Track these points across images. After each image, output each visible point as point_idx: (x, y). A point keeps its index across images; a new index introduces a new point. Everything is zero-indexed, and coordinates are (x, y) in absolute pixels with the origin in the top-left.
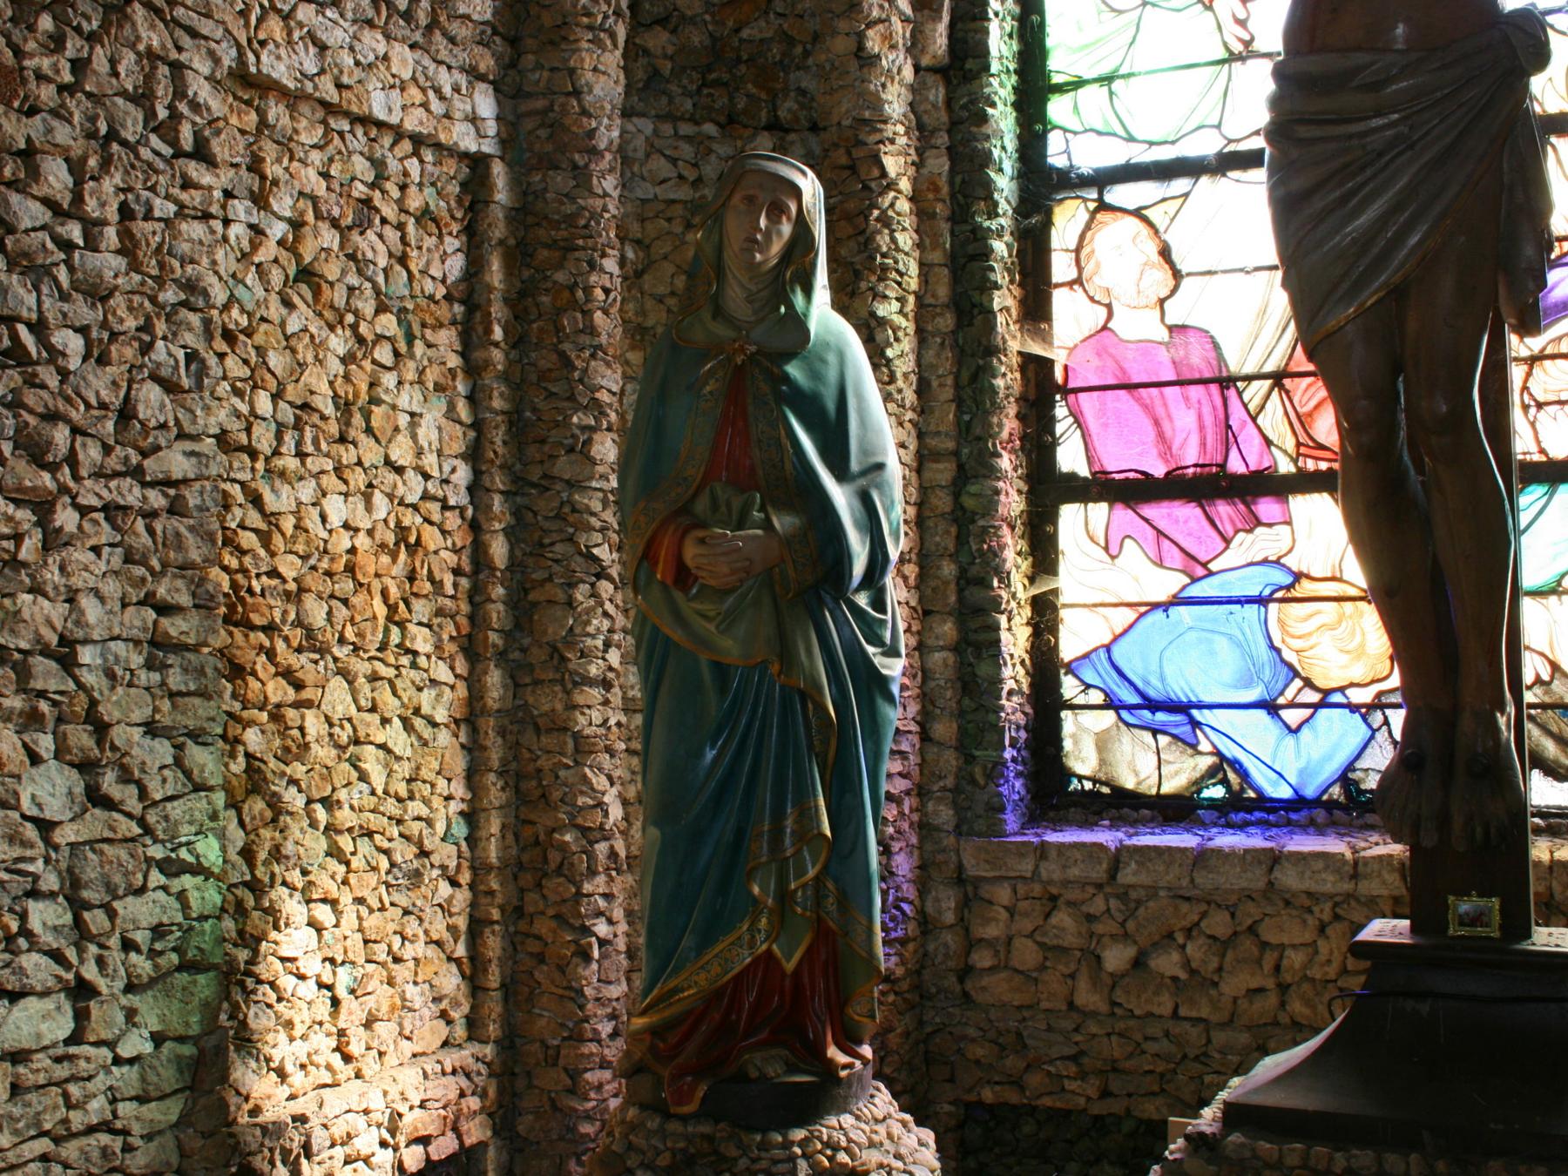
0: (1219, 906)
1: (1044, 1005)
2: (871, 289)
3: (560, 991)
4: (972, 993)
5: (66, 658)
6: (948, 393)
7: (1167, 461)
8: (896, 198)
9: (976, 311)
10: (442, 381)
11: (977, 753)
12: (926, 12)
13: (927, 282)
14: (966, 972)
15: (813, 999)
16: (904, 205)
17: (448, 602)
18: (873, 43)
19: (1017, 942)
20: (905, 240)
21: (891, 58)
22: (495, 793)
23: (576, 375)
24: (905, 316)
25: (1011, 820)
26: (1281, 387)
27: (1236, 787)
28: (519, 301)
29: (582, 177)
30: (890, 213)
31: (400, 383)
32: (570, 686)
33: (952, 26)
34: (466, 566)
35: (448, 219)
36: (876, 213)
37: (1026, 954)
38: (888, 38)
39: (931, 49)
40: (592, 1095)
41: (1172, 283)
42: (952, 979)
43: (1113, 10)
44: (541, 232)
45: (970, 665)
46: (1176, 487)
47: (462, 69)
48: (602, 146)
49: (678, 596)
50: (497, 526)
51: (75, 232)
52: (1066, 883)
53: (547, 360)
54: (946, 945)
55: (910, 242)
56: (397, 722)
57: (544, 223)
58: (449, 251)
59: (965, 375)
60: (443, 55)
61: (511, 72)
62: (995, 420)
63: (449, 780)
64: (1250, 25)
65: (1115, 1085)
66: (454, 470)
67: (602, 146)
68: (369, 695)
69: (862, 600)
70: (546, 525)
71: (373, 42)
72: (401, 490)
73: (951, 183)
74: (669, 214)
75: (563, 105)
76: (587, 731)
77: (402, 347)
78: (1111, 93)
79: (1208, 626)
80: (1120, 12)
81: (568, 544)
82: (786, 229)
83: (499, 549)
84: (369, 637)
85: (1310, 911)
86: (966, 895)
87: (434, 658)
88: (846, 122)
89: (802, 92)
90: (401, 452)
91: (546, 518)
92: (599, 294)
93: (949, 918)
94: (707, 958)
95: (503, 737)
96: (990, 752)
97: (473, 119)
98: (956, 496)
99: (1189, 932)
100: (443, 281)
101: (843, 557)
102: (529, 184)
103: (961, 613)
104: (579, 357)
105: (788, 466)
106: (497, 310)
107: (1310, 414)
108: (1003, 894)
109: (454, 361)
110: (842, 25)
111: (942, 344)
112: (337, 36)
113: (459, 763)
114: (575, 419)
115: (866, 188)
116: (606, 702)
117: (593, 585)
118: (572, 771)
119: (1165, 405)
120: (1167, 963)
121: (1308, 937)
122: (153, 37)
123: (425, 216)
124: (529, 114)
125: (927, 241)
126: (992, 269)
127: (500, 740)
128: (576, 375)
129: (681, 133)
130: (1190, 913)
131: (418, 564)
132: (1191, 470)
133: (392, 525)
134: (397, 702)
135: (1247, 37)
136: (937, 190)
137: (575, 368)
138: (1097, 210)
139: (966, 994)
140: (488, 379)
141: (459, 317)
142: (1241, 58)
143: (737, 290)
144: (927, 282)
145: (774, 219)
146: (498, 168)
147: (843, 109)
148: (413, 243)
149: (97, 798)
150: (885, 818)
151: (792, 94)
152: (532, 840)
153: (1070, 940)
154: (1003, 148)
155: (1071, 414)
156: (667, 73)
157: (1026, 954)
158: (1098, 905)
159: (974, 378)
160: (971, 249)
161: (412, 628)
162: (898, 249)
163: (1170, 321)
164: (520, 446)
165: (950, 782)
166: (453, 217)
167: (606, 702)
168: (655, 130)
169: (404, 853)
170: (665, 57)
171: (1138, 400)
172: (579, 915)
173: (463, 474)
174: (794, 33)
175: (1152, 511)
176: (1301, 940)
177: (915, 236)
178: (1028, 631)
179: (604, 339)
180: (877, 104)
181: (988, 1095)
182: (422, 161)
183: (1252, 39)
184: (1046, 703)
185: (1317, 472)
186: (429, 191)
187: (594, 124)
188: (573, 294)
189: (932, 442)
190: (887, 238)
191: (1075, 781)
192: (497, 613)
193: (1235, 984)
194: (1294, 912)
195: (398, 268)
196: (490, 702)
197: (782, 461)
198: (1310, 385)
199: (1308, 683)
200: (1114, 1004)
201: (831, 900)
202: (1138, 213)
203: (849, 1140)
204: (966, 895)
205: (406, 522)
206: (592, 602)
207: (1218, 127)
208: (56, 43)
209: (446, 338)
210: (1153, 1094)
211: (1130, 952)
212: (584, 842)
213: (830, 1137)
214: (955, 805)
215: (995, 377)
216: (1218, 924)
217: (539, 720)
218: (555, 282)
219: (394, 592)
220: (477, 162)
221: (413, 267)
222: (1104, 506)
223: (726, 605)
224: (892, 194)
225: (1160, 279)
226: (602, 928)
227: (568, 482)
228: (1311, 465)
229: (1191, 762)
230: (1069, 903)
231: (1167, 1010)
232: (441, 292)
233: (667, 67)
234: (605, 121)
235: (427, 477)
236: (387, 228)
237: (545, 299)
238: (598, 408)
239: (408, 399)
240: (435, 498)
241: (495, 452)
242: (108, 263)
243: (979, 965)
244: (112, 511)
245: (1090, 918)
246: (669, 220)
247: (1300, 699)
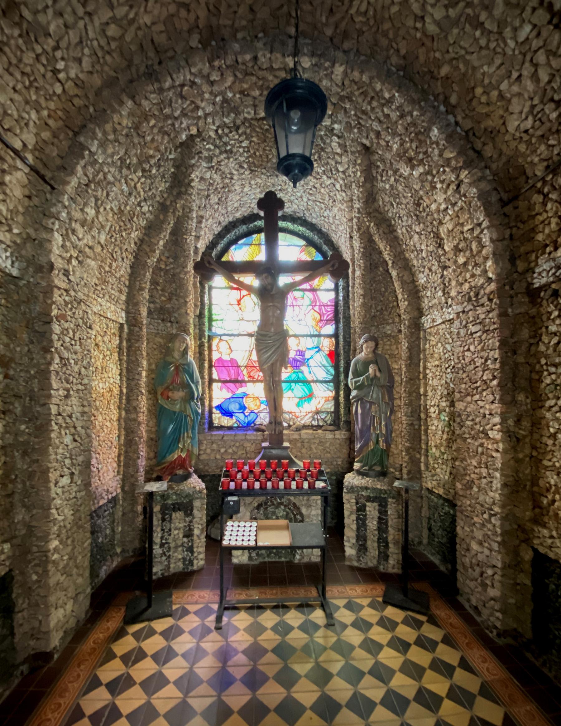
5: (70, 417)
22: (123, 432)
25: (206, 430)
28: (129, 348)
29: (141, 329)
37: (208, 451)
46: (230, 381)
51: (73, 342)
53: (134, 359)
71: (108, 304)
83: (125, 391)
90: (110, 375)
106: (125, 350)
112: (103, 304)
113: (117, 427)
120: (230, 451)
122: (84, 308)
123: (114, 334)
130: (233, 443)
146: (125, 327)
147: (183, 321)
149: (75, 440)
157: (208, 451)
164: (129, 373)
169: (109, 444)
184: (211, 413)
192: (124, 401)
193: (240, 453)
208: (71, 309)
209: (116, 354)
216: (237, 444)
220: (122, 325)
225: (229, 351)
239: (111, 366)
242: (78, 347)
244: (78, 390)
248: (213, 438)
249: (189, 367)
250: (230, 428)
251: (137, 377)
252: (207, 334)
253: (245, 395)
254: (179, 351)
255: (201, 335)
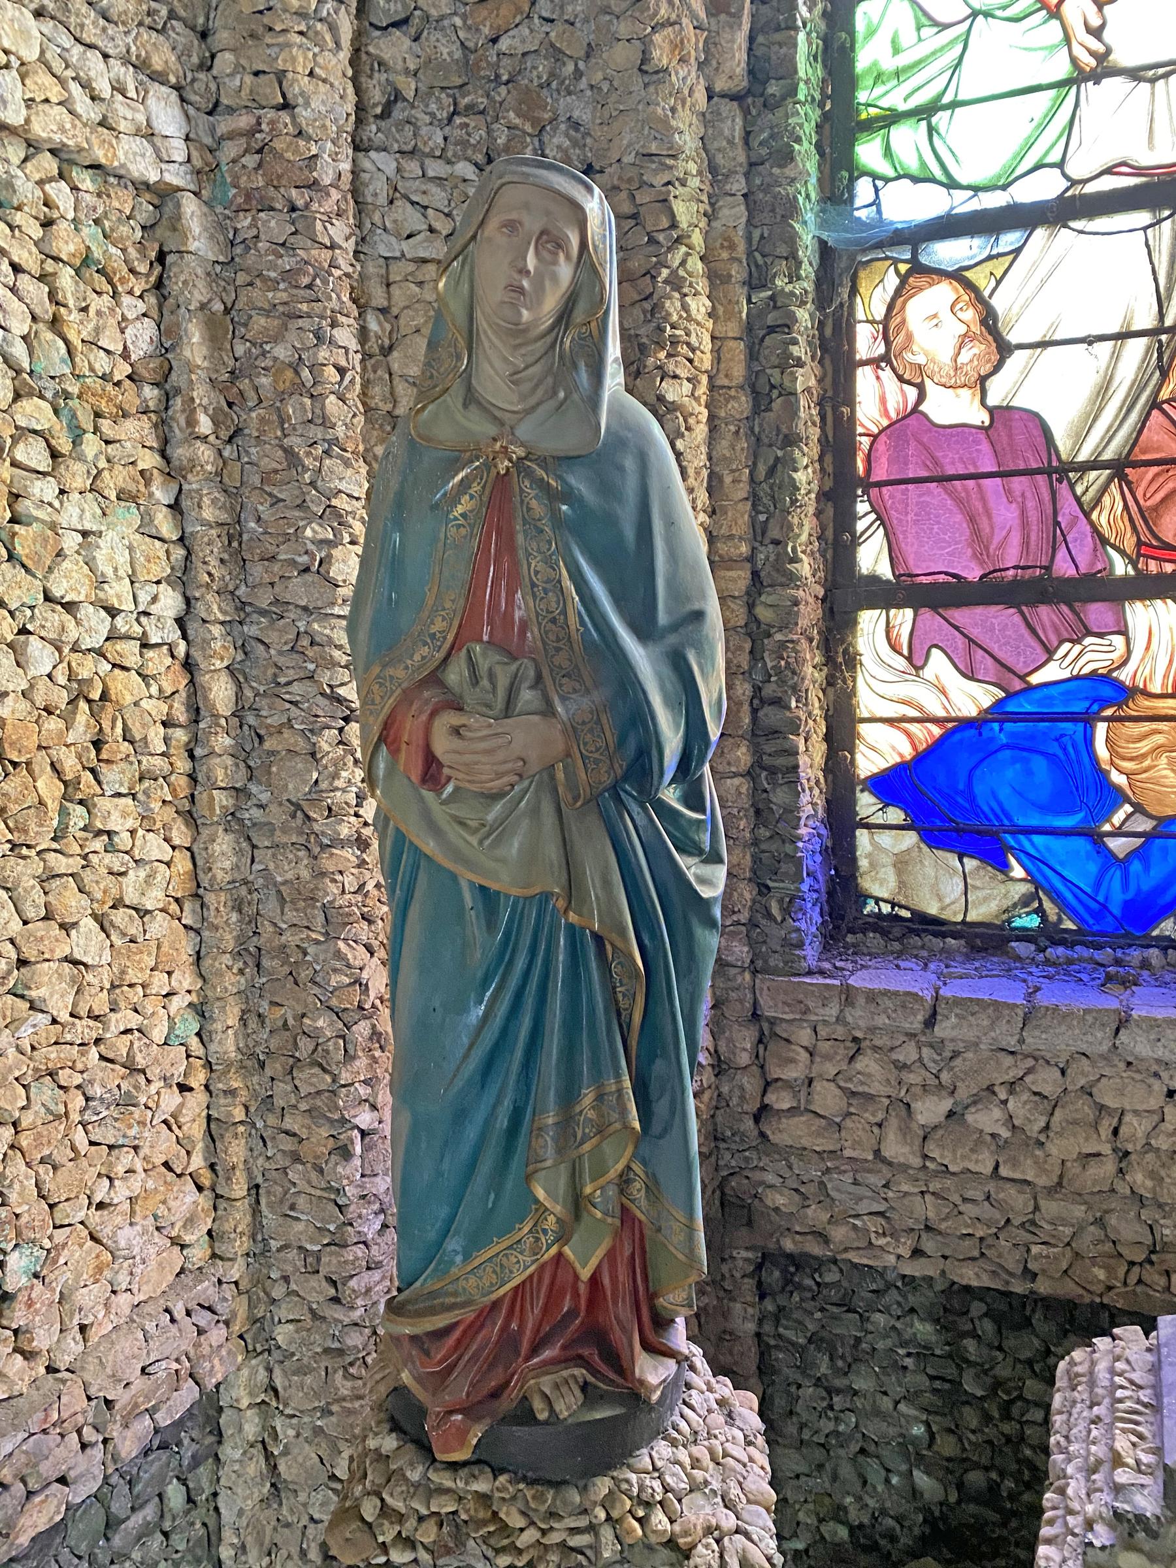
0: (1048, 1062)
1: (847, 1153)
2: (659, 368)
3: (319, 1193)
4: (769, 1133)
6: (743, 490)
7: (982, 563)
8: (688, 254)
9: (775, 393)
10: (132, 487)
11: (771, 884)
12: (723, 17)
13: (719, 360)
14: (762, 1113)
15: (615, 1303)
16: (696, 265)
17: (158, 761)
18: (661, 55)
19: (818, 1086)
20: (699, 306)
21: (681, 74)
23: (307, 477)
24: (697, 399)
25: (810, 954)
26: (1123, 478)
27: (1053, 918)
28: (231, 387)
30: (681, 273)
31: (62, 492)
32: (316, 850)
33: (751, 39)
34: (181, 714)
35: (125, 270)
36: (665, 272)
37: (827, 1099)
38: (678, 45)
39: (727, 67)
40: (359, 1302)
41: (995, 357)
42: (750, 1123)
43: (936, 24)
44: (255, 293)
45: (765, 791)
46: (992, 591)
47: (126, 61)
48: (327, 181)
49: (428, 795)
50: (219, 664)
52: (872, 1030)
54: (742, 1088)
55: (703, 310)
56: (88, 924)
57: (258, 282)
58: (130, 315)
59: (762, 469)
60: (91, 34)
61: (202, 76)
62: (796, 521)
63: (169, 973)
64: (1106, 35)
65: (928, 1245)
66: (155, 599)
67: (327, 181)
68: (41, 900)
69: (670, 795)
70: (281, 661)
72: (73, 633)
73: (749, 239)
74: (420, 278)
75: (272, 122)
76: (340, 902)
77: (64, 444)
78: (931, 130)
79: (1027, 744)
80: (946, 26)
81: (307, 682)
82: (565, 271)
83: (221, 693)
84: (33, 827)
85: (1156, 1075)
86: (762, 1033)
87: (140, 832)
88: (628, 159)
89: (576, 125)
90: (69, 581)
91: (280, 653)
92: (331, 373)
93: (744, 1059)
94: (476, 1263)
95: (240, 911)
96: (786, 885)
97: (149, 134)
98: (751, 607)
99: (1011, 1086)
100: (125, 354)
101: (649, 746)
102: (236, 230)
103: (754, 734)
104: (308, 454)
105: (573, 620)
106: (201, 393)
107: (1155, 509)
108: (804, 1036)
109: (149, 460)
110: (623, 28)
111: (737, 432)
114: (308, 533)
115: (652, 241)
116: (362, 864)
117: (341, 730)
118: (323, 947)
119: (983, 499)
120: (987, 1119)
121: (1154, 1103)
124: (231, 136)
125: (720, 310)
126: (795, 342)
127: (234, 917)
128: (307, 477)
129: (431, 173)
130: (1009, 1069)
131: (106, 725)
132: (1011, 572)
133: (62, 679)
134: (85, 901)
135: (1101, 49)
136: (732, 247)
137: (306, 469)
138: (909, 273)
139: (762, 1135)
140: (193, 483)
141: (152, 405)
142: (1096, 76)
143: (498, 364)
144: (719, 360)
145: (547, 264)
146: (190, 207)
148: (71, 303)
150: (699, 1064)
151: (563, 127)
152: (280, 1023)
153: (876, 1088)
154: (808, 196)
155: (874, 510)
156: (410, 94)
157: (827, 1099)
158: (908, 1053)
159: (771, 471)
160: (770, 319)
161: (104, 804)
162: (689, 318)
163: (992, 401)
165: (744, 917)
166: (132, 271)
167: (362, 864)
168: (398, 170)
170: (407, 71)
171: (951, 494)
172: (337, 1108)
173: (170, 602)
174: (563, 46)
175: (960, 615)
176: (1145, 1107)
177: (708, 303)
178: (824, 746)
179: (340, 431)
180: (663, 130)
181: (788, 1245)
182: (75, 189)
183: (1109, 51)
184: (841, 823)
185: (1161, 576)
186: (90, 231)
187: (314, 151)
188: (297, 373)
189: (722, 548)
190: (678, 304)
191: (872, 902)
192: (222, 770)
193: (1061, 1148)
194: (1138, 1077)
195: (49, 336)
196: (220, 875)
197: (564, 612)
198: (1157, 475)
199: (1139, 809)
200: (925, 1157)
201: (637, 1185)
202: (958, 276)
203: (667, 1489)
204: (762, 1033)
205: (84, 674)
206: (340, 750)
207: (1060, 165)
210: (973, 1259)
211: (947, 1104)
212: (341, 1025)
213: (641, 1488)
214: (751, 943)
215: (796, 470)
216: (1047, 1081)
217: (282, 888)
218: (275, 359)
219: (70, 764)
220: (162, 195)
221: (72, 336)
222: (909, 613)
223: (490, 817)
224: (683, 249)
226: (365, 1118)
227: (305, 609)
228: (1153, 567)
229: (1002, 889)
230: (876, 1049)
231: (988, 1169)
232: (122, 371)
233: (408, 88)
234: (329, 145)
235: (112, 612)
236: (24, 279)
237: (265, 381)
238: (337, 518)
239: (78, 512)
240: (127, 637)
241: (210, 574)
243: (776, 1106)
245: (902, 1067)
246: (420, 284)
247: (1127, 828)
248: (858, 1017)
249: (608, 489)
250: (987, 942)
251: (299, 591)
252: (808, 233)
253: (1107, 693)
254: (517, 333)
255: (763, 248)
